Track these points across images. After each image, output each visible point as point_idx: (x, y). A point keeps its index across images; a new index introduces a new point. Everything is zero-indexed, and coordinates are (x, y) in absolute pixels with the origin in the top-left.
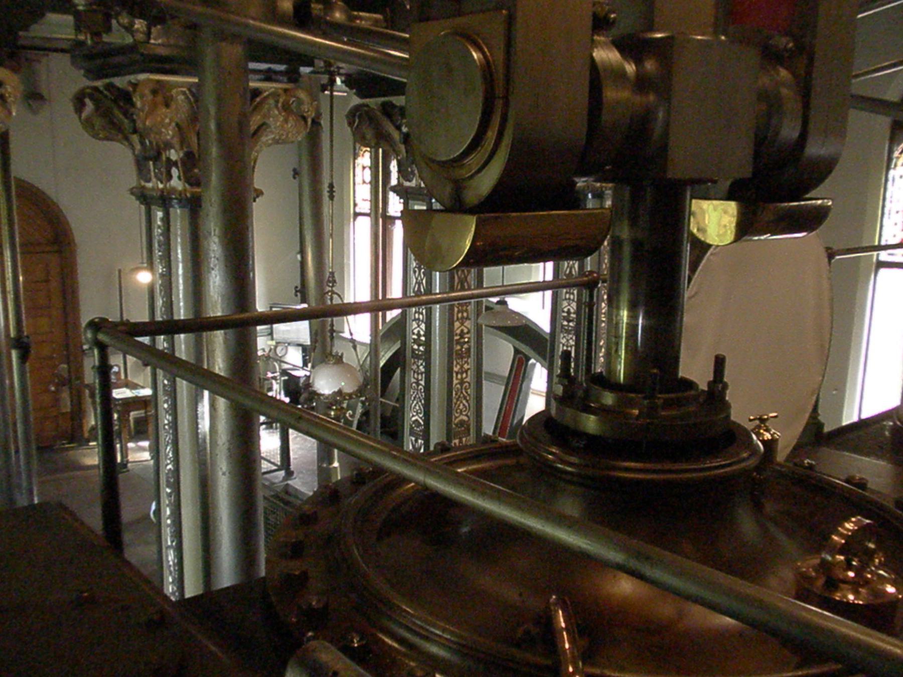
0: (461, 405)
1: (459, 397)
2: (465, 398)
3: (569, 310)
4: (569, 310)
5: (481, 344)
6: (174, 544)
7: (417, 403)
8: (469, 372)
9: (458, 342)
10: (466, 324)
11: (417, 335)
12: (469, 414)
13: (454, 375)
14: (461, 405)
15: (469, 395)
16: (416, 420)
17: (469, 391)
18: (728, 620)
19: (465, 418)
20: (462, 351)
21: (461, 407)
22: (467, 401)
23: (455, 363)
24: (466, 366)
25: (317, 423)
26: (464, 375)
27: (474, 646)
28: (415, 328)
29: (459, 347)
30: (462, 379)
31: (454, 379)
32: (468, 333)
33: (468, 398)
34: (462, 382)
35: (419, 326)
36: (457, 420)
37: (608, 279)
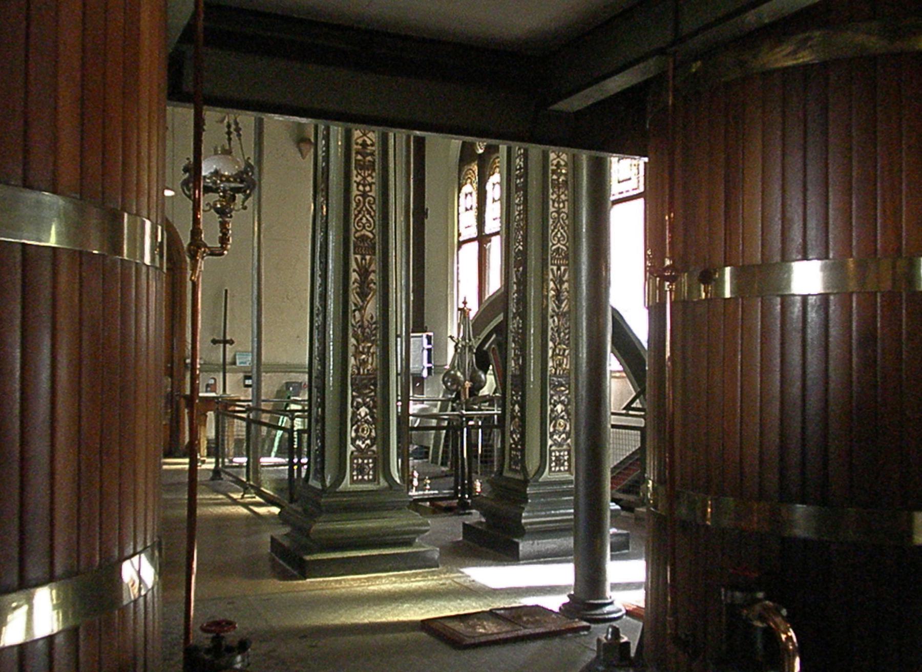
0: (364, 219)
1: (362, 209)
2: (369, 213)
3: (558, 162)
4: (558, 162)
5: (201, 141)
6: (784, 637)
7: (559, 231)
8: (373, 186)
9: (554, 172)
10: (369, 135)
11: (556, 166)
12: (374, 231)
13: (551, 203)
14: (364, 219)
15: (374, 211)
16: (559, 248)
17: (374, 206)
18: (187, 440)
19: (371, 236)
20: (558, 182)
21: (364, 221)
22: (372, 217)
23: (551, 191)
24: (563, 197)
25: (135, 239)
26: (368, 188)
27: (677, 546)
28: (555, 159)
29: (555, 177)
30: (559, 208)
31: (551, 207)
32: (372, 145)
33: (373, 214)
34: (364, 195)
35: (558, 157)
36: (358, 235)
37: (594, 153)
